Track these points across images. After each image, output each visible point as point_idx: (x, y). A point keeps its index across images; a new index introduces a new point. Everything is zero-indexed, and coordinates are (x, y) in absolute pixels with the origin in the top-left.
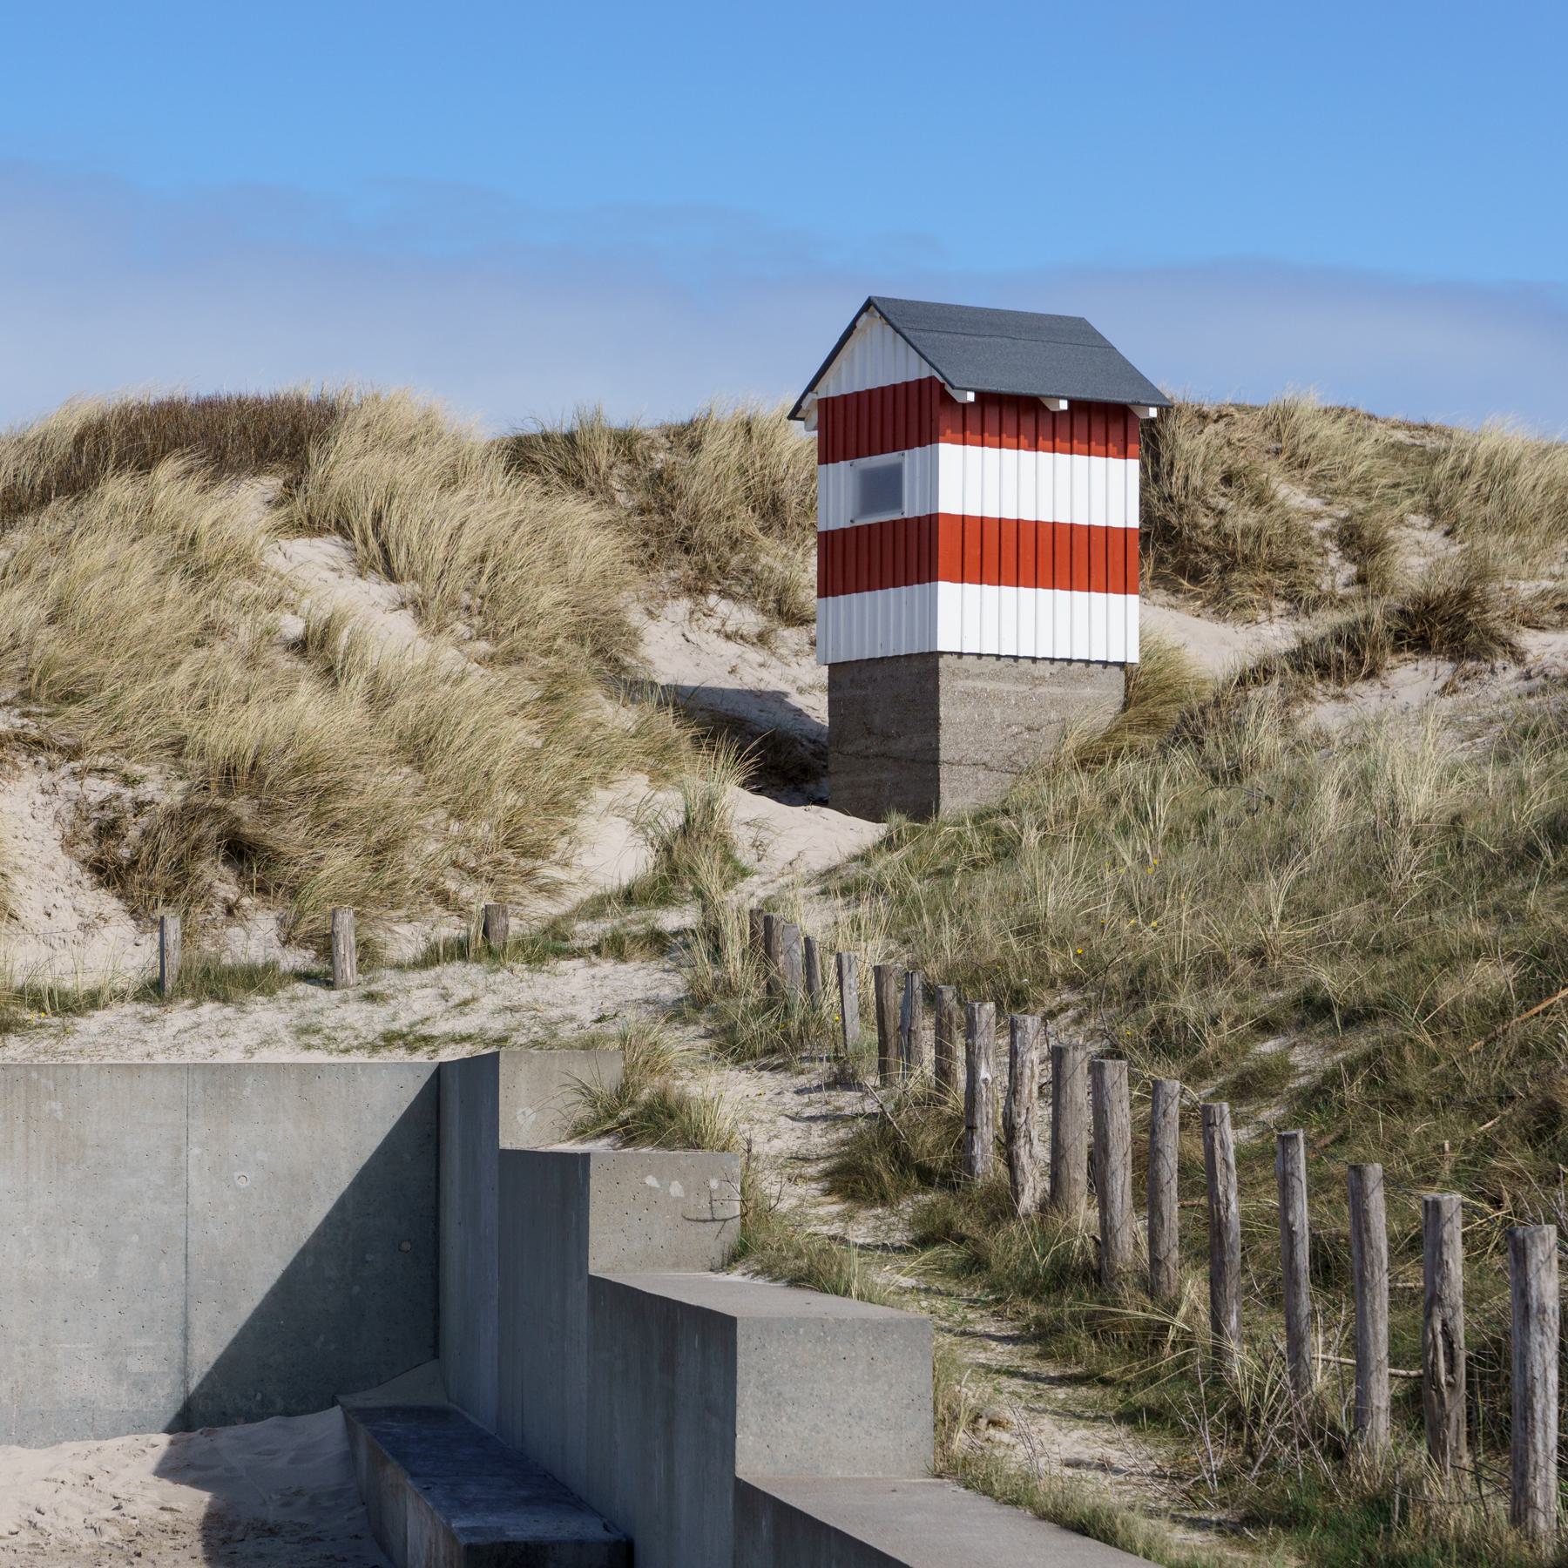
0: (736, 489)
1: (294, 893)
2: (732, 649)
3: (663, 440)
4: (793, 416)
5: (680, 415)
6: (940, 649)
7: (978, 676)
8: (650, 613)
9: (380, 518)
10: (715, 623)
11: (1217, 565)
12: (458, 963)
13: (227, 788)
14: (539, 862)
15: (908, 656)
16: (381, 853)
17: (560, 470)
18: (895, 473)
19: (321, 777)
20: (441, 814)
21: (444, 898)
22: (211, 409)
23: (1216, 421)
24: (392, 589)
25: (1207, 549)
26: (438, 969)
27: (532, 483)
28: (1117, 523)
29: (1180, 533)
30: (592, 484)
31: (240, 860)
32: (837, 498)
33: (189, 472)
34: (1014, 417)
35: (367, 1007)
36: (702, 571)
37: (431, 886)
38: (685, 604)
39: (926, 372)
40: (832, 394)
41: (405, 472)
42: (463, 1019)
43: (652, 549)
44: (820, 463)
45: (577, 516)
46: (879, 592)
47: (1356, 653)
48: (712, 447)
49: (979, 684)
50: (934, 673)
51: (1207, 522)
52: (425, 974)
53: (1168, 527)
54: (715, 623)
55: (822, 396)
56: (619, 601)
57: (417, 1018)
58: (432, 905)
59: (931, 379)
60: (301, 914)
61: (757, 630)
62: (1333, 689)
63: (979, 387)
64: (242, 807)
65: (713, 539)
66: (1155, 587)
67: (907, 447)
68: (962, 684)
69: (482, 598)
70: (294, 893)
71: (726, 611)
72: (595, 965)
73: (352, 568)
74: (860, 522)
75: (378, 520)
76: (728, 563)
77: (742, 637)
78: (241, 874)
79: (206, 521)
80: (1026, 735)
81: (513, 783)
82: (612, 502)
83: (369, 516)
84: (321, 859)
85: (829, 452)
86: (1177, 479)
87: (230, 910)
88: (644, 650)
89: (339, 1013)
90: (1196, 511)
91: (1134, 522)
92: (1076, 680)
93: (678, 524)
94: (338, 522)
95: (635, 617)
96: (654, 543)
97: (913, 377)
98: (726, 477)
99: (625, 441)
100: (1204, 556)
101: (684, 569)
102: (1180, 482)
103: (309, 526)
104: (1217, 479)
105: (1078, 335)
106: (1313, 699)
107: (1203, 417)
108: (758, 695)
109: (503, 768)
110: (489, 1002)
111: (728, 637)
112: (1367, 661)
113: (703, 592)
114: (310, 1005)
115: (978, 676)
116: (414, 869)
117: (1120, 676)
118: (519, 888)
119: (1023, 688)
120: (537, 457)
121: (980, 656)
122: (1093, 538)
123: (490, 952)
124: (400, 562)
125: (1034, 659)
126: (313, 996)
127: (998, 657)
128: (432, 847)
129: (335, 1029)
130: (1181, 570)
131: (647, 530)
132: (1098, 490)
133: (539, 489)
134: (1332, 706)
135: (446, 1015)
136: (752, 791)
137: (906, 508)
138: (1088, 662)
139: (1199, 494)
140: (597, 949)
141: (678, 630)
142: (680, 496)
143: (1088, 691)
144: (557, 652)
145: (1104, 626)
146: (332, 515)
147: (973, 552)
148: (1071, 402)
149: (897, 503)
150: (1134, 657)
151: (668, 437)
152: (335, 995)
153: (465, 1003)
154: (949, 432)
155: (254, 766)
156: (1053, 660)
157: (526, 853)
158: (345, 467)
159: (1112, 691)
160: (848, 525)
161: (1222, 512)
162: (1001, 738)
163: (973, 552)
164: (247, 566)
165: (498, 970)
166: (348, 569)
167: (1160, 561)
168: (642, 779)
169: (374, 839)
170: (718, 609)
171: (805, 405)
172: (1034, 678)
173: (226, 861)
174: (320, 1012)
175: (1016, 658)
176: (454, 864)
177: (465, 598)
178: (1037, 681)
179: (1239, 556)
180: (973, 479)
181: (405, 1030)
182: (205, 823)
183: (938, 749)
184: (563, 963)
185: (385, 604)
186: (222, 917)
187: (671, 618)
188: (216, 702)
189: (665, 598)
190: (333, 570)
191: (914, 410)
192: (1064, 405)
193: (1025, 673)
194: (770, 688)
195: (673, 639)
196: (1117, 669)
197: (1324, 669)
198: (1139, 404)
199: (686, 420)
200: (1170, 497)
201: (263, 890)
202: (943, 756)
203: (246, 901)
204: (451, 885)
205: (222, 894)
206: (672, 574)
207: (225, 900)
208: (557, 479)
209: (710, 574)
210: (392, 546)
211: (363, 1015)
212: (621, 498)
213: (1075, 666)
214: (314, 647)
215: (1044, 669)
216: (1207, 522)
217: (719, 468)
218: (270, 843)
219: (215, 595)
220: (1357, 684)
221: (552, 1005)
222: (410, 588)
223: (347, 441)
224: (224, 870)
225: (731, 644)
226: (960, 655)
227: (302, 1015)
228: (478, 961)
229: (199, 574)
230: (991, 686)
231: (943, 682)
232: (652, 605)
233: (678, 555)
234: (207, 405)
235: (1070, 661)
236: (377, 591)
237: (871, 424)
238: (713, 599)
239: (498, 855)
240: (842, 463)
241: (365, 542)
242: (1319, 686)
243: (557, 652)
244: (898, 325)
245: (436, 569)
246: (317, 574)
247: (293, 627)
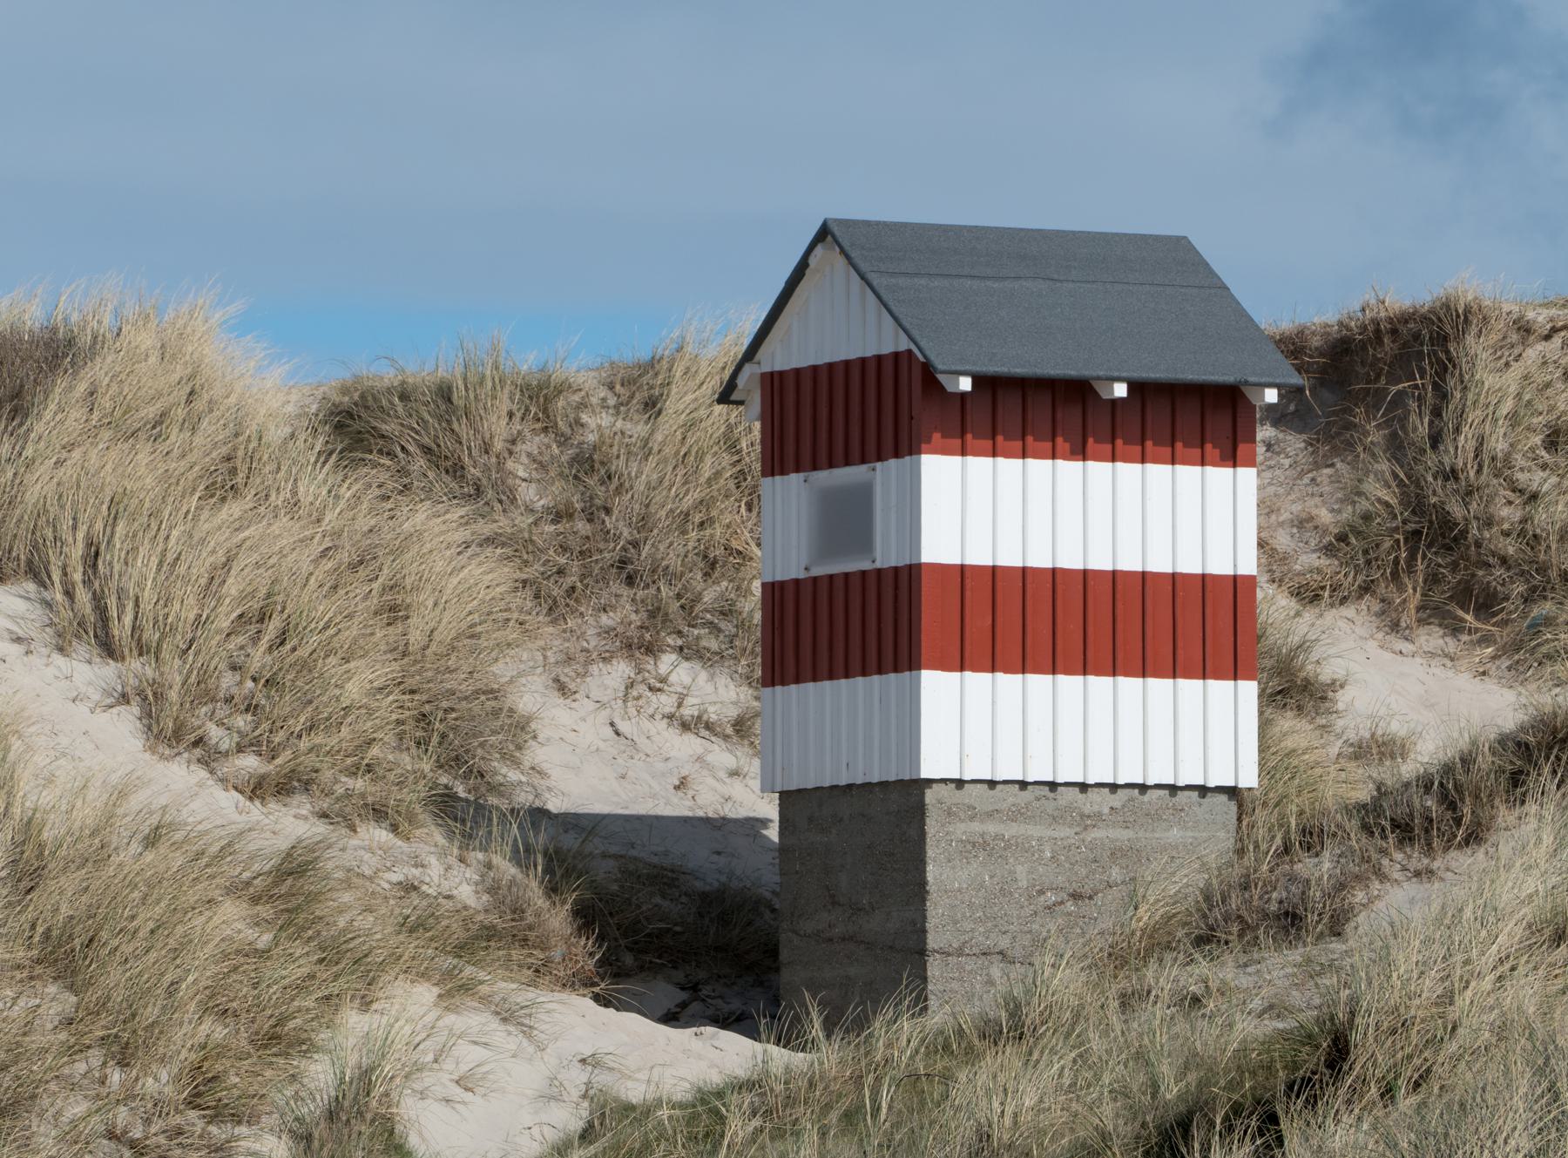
0: (718, 474)
2: (686, 746)
3: (603, 392)
6: (924, 775)
7: (990, 815)
8: (562, 688)
9: (97, 554)
10: (666, 702)
11: (1519, 588)
14: (243, 1130)
15: (884, 785)
17: (427, 450)
18: (864, 495)
23: (1547, 338)
24: (109, 671)
25: (1504, 561)
27: (378, 474)
29: (1464, 533)
30: (476, 472)
32: (782, 532)
36: (652, 614)
38: (621, 670)
39: (887, 341)
40: (779, 366)
41: (140, 472)
43: (572, 579)
44: (764, 474)
47: (1452, 806)
48: (677, 404)
49: (992, 828)
50: (920, 811)
51: (1508, 514)
53: (1447, 522)
54: (666, 702)
55: (766, 368)
56: (502, 670)
61: (733, 713)
62: (1418, 860)
65: (673, 561)
67: (880, 459)
68: (961, 829)
69: (254, 680)
71: (687, 680)
75: (92, 557)
76: (698, 598)
80: (1070, 906)
83: (77, 552)
86: (1467, 440)
88: (536, 754)
92: (1154, 817)
93: (617, 538)
94: (30, 563)
95: (531, 696)
96: (575, 567)
97: (887, 349)
99: (540, 399)
100: (1499, 572)
101: (625, 612)
102: (1472, 444)
105: (1173, 265)
106: (1382, 877)
107: (1525, 329)
108: (718, 826)
109: (197, 976)
111: (685, 726)
112: (1467, 819)
113: (651, 650)
115: (990, 815)
119: (1063, 832)
120: (388, 428)
121: (992, 784)
124: (121, 630)
125: (1083, 787)
127: (1023, 785)
128: (77, 1108)
130: (1464, 595)
131: (564, 549)
132: (1188, 517)
134: (1412, 888)
136: (596, 998)
137: (878, 554)
138: (1173, 789)
142: (619, 491)
143: (1175, 834)
144: (369, 769)
145: (1198, 731)
147: (979, 622)
148: (1134, 386)
149: (864, 543)
150: (1249, 778)
151: (611, 387)
154: (937, 436)
156: (1114, 787)
157: (217, 1115)
159: (1213, 835)
160: (802, 575)
161: (1534, 497)
162: (1028, 911)
163: (979, 622)
167: (1433, 579)
170: (673, 678)
171: (741, 381)
172: (1082, 816)
175: (1053, 785)
176: (111, 1135)
177: (228, 681)
179: (1553, 574)
180: (975, 509)
183: (924, 931)
185: (96, 697)
187: (595, 694)
189: (588, 662)
190: (18, 640)
192: (1120, 390)
193: (1069, 808)
195: (594, 732)
196: (1223, 798)
197: (1404, 831)
198: (1246, 383)
199: (644, 355)
200: (1453, 471)
202: (933, 941)
206: (605, 620)
208: (420, 463)
209: (666, 619)
210: (112, 603)
213: (1153, 795)
215: (1100, 802)
216: (1508, 514)
220: (1453, 854)
222: (137, 667)
226: (960, 783)
230: (1012, 830)
231: (931, 827)
232: (566, 674)
233: (618, 587)
235: (1143, 788)
236: (87, 672)
237: (844, 414)
238: (667, 660)
240: (793, 476)
241: (69, 594)
242: (1399, 856)
243: (369, 769)
244: (863, 266)
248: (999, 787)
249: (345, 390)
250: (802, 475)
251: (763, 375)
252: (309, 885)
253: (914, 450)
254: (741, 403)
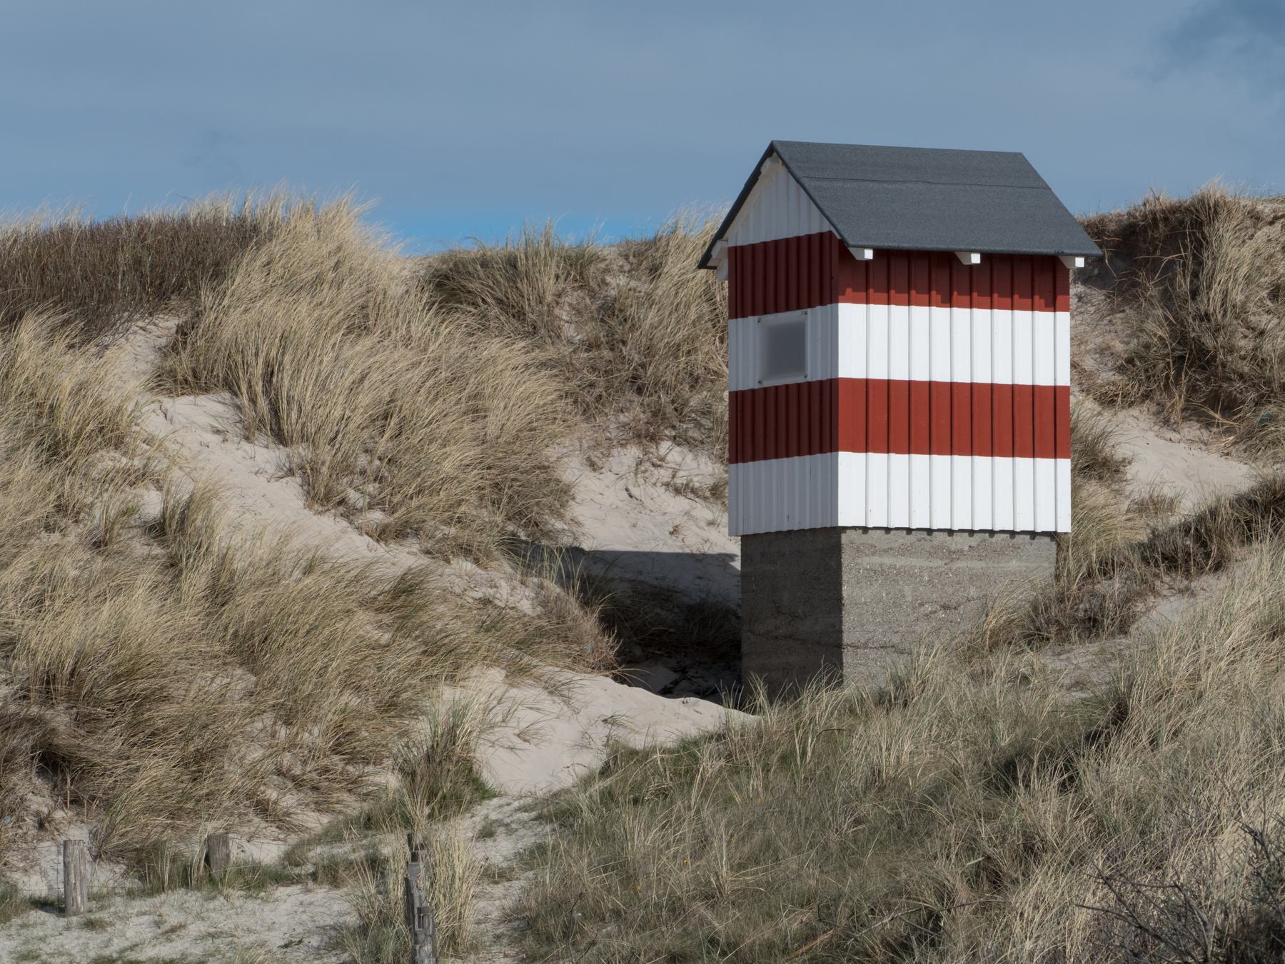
1: (107, 805)
2: (682, 503)
5: (642, 230)
6: (841, 524)
7: (886, 551)
10: (664, 475)
11: (1252, 395)
12: (182, 891)
13: (47, 698)
14: (370, 768)
15: (813, 530)
16: (199, 763)
19: (142, 685)
20: (268, 718)
21: (263, 809)
22: (103, 239)
23: (1271, 223)
25: (1241, 376)
26: (163, 896)
27: (465, 318)
29: (1214, 357)
30: (534, 317)
31: (55, 772)
32: (741, 357)
33: (66, 323)
35: (87, 934)
36: (655, 414)
37: (249, 796)
38: (633, 452)
41: (303, 314)
42: (169, 945)
43: (597, 391)
44: (730, 317)
45: (503, 355)
46: (785, 459)
47: (1204, 545)
49: (887, 560)
50: (837, 549)
52: (150, 901)
53: (1201, 350)
54: (664, 475)
55: (732, 244)
56: (551, 453)
57: (127, 944)
58: (251, 816)
60: (112, 827)
61: (710, 482)
62: (1181, 583)
63: (877, 244)
64: (60, 718)
65: (669, 377)
66: (1185, 419)
67: (810, 306)
68: (867, 561)
70: (107, 805)
71: (679, 459)
72: (309, 891)
73: (238, 429)
74: (768, 383)
76: (686, 403)
77: (693, 491)
78: (55, 786)
79: (67, 382)
80: (941, 614)
81: (351, 682)
82: (556, 334)
83: (259, 370)
84: (137, 770)
85: (741, 306)
86: (1216, 292)
87: (42, 823)
89: (61, 939)
90: (1233, 333)
92: (999, 552)
94: (225, 379)
95: (571, 471)
96: (602, 382)
97: (815, 230)
98: (688, 306)
99: (578, 266)
100: (1238, 384)
101: (636, 413)
103: (195, 383)
104: (1264, 293)
105: (1012, 173)
107: (1256, 218)
110: (195, 928)
111: (677, 491)
113: (654, 438)
114: (38, 932)
115: (886, 551)
116: (234, 777)
117: (1049, 546)
118: (345, 796)
119: (937, 563)
121: (888, 530)
122: (1017, 399)
123: (211, 880)
124: (291, 421)
125: (951, 532)
126: (43, 923)
127: (909, 531)
129: (52, 955)
130: (1214, 400)
132: (1024, 346)
135: (154, 942)
137: (809, 372)
138: (1013, 533)
139: (1240, 313)
140: (314, 876)
141: (621, 483)
145: (1028, 493)
146: (220, 372)
149: (800, 365)
150: (1065, 526)
151: (627, 257)
152: (62, 922)
153: (173, 930)
154: (849, 290)
155: (72, 674)
157: (352, 758)
158: (245, 310)
160: (757, 386)
162: (912, 618)
164: (112, 433)
165: (214, 898)
166: (235, 431)
167: (1193, 390)
168: (497, 674)
169: (192, 748)
170: (669, 458)
171: (715, 253)
172: (950, 552)
173: (41, 772)
174: (42, 939)
175: (930, 531)
176: (279, 773)
177: (363, 460)
178: (954, 555)
179: (1276, 386)
180: (876, 341)
181: (115, 955)
182: (21, 733)
183: (841, 632)
184: (281, 889)
186: (33, 832)
188: (52, 599)
189: (611, 447)
190: (218, 432)
191: (816, 266)
194: (716, 550)
195: (615, 496)
196: (1047, 539)
199: (650, 236)
201: (76, 801)
202: (847, 638)
203: (59, 814)
204: (272, 794)
205: (34, 807)
207: (38, 813)
208: (496, 310)
211: (81, 941)
212: (569, 331)
213: (997, 538)
214: (173, 531)
215: (962, 542)
216: (1244, 344)
217: (681, 294)
218: (84, 754)
219: (70, 471)
220: (1204, 578)
221: (249, 931)
222: (301, 451)
223: (247, 276)
224: (38, 782)
225: (680, 499)
227: (26, 942)
228: (198, 889)
229: (54, 450)
230: (901, 562)
231: (846, 559)
232: (596, 456)
233: (631, 395)
234: (95, 235)
235: (992, 533)
236: (266, 454)
237: (786, 276)
238: (665, 446)
239: (326, 762)
240: (751, 318)
241: (253, 401)
242: (1167, 579)
243: (459, 520)
245: (329, 431)
246: (196, 442)
247: (152, 503)
250: (756, 318)
251: (730, 249)
253: (834, 300)
254: (715, 268)
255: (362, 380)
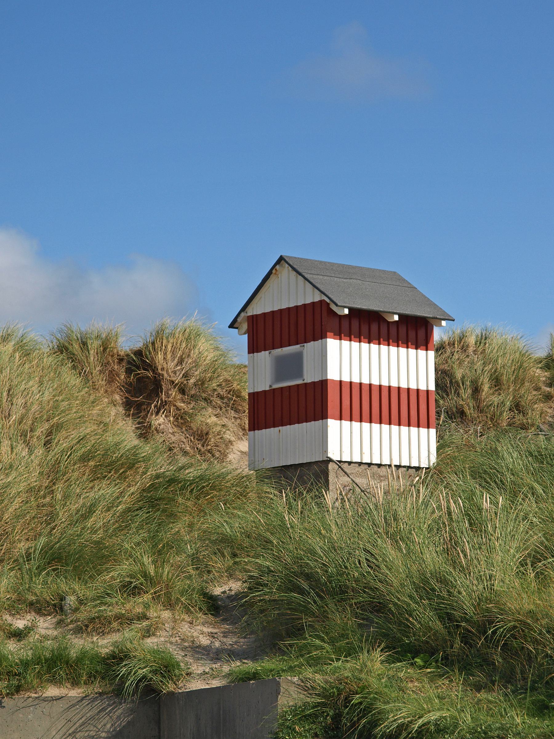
4: (232, 326)
28: (423, 387)
32: (260, 373)
34: (367, 325)
59: (321, 302)
74: (275, 386)
85: (254, 347)
91: (432, 387)
132: (410, 369)
133: (120, 353)
137: (305, 377)
145: (416, 446)
149: (299, 373)
160: (267, 389)
168: (378, 656)
171: (239, 320)
180: (346, 360)
198: (436, 318)
237: (285, 329)
248: (372, 466)
249: (61, 331)
250: (267, 352)
251: (248, 317)
252: (139, 432)
253: (323, 336)
254: (237, 328)
255: (185, 331)
